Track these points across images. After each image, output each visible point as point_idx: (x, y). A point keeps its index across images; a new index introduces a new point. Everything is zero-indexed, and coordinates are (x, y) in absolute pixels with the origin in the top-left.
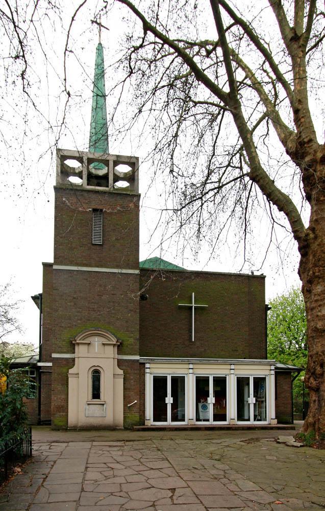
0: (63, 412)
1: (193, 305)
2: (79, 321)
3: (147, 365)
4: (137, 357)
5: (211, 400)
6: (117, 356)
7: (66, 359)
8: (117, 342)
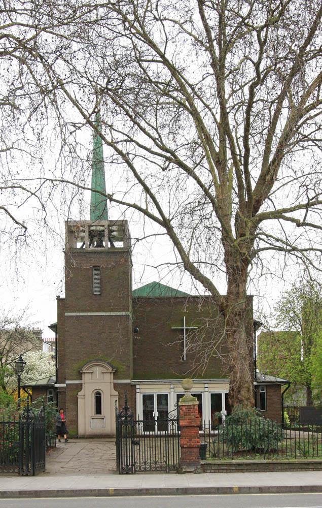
0: (74, 425)
1: (185, 328)
2: (85, 355)
3: (138, 387)
4: (128, 381)
5: (156, 414)
6: (113, 381)
7: (77, 384)
8: (113, 370)
